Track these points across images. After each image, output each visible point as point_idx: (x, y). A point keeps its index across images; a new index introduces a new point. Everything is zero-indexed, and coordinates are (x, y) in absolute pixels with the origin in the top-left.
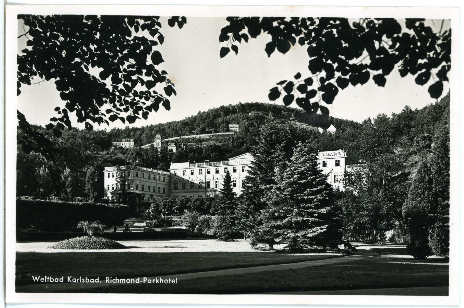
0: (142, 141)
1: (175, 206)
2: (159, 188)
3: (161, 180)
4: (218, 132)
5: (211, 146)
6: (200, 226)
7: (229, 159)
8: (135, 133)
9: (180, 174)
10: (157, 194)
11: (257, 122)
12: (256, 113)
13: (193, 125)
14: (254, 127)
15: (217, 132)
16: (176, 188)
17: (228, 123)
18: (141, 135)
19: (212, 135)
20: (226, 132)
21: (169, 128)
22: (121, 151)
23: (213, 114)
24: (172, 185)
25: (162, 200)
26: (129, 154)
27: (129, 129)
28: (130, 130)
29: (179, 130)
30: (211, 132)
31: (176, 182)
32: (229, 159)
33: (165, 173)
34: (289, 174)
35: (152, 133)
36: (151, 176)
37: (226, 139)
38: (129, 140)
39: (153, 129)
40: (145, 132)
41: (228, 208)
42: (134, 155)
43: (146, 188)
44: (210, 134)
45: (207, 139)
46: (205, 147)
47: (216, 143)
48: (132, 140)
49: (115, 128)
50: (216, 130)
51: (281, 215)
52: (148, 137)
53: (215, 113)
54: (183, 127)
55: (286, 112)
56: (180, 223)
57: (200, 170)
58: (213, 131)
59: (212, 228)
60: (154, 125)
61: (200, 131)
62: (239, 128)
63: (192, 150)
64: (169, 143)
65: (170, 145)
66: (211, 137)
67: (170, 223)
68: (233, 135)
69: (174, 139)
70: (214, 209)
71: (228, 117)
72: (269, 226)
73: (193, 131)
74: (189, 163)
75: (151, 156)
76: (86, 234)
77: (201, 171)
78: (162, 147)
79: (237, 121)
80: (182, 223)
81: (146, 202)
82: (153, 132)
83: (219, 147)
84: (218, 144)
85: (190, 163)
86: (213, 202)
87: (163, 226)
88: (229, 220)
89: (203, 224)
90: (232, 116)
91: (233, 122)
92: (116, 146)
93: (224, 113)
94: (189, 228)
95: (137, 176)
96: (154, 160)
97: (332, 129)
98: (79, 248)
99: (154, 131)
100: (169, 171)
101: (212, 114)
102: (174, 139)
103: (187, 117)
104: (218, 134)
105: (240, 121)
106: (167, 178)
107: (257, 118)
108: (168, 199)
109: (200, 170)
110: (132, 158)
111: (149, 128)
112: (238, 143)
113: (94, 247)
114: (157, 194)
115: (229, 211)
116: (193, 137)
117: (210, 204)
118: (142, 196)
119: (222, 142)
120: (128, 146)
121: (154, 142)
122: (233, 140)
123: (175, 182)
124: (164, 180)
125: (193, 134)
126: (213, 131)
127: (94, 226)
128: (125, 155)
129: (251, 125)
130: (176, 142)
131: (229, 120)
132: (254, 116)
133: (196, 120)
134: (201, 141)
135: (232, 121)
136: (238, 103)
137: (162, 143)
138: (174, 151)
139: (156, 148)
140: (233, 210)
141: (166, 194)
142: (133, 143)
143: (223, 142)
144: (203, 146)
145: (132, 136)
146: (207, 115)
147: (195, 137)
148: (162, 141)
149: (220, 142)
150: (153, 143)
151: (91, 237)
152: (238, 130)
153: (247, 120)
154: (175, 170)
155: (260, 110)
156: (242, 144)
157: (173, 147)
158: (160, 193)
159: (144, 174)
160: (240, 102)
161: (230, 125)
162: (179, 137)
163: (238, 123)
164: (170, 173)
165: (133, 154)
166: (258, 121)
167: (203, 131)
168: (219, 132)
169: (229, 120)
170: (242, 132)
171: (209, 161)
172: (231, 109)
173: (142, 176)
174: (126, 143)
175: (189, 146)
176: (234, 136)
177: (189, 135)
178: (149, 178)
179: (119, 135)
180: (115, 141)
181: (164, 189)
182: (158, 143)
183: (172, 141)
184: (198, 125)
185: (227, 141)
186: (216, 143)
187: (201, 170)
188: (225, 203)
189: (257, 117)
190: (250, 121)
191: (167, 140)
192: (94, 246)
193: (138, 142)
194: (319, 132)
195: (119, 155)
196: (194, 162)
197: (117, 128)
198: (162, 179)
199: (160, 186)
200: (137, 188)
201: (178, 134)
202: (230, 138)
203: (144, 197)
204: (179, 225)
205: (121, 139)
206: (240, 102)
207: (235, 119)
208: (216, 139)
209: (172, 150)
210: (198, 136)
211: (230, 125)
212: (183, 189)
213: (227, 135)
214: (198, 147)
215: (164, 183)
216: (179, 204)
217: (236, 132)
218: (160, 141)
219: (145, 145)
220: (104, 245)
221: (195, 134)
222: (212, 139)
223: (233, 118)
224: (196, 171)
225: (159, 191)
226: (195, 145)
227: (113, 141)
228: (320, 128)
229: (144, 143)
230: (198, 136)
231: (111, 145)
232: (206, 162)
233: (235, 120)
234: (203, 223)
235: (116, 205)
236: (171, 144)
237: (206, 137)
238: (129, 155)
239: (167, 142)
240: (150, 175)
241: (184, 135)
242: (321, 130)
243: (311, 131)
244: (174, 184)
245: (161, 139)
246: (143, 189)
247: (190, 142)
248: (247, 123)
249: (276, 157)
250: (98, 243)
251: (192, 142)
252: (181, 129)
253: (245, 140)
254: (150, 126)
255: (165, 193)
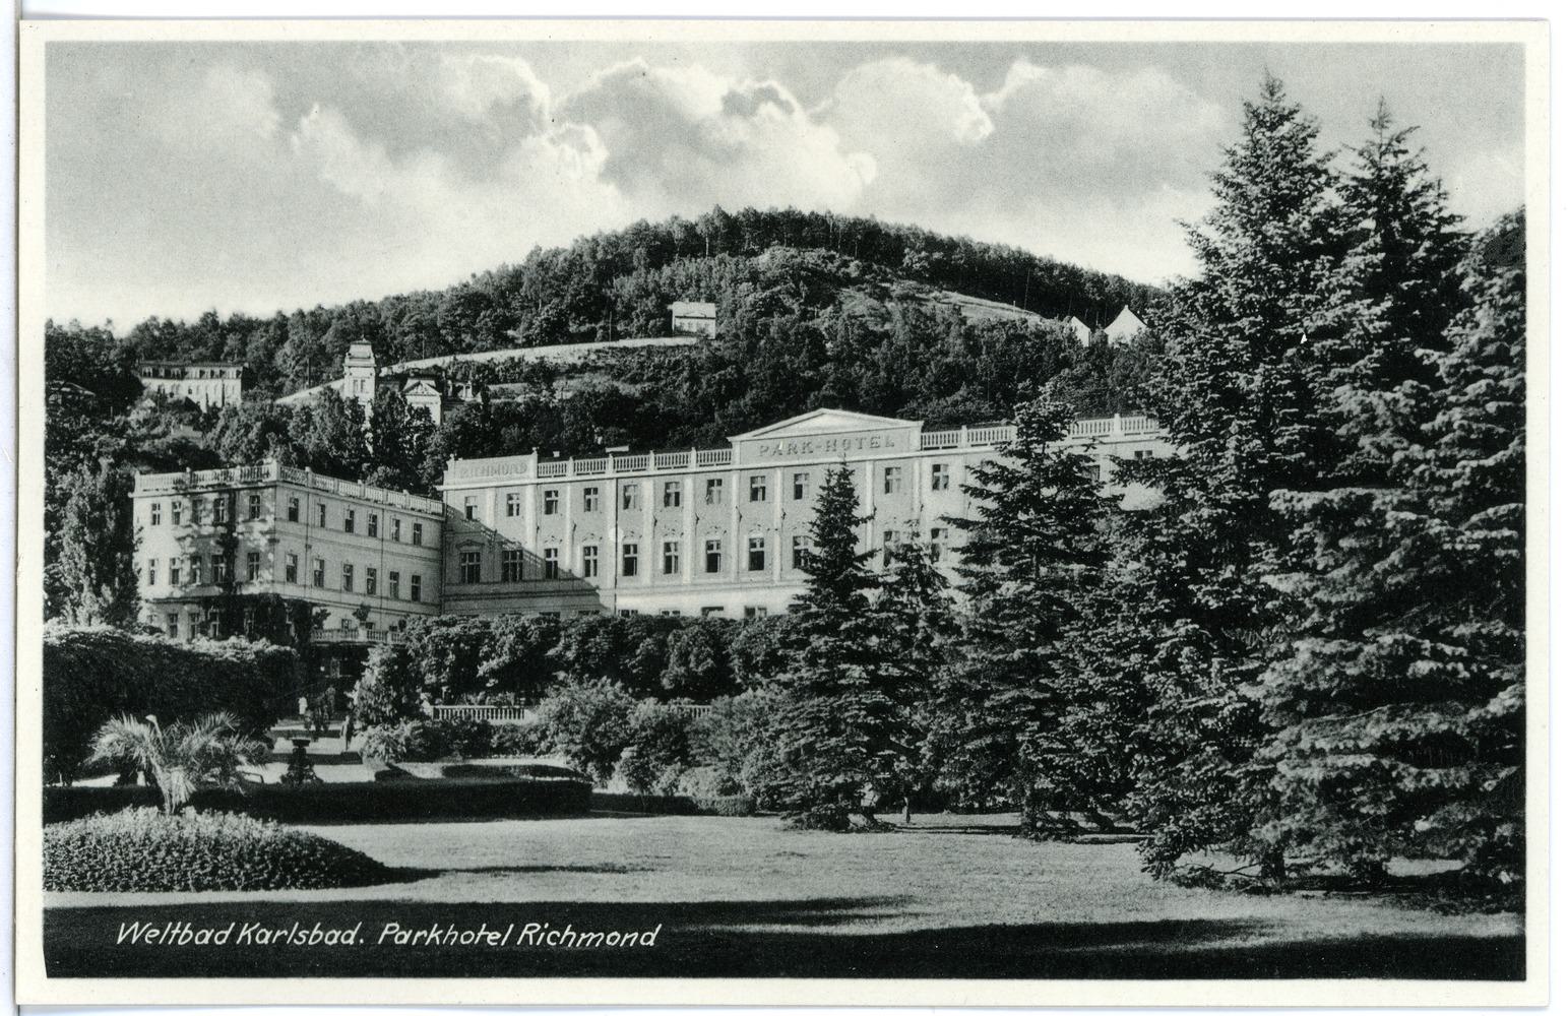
0: (278, 374)
1: (487, 657)
2: (394, 576)
3: (402, 539)
4: (623, 338)
5: (597, 395)
6: (640, 755)
7: (729, 439)
8: (244, 344)
9: (489, 515)
10: (385, 604)
11: (795, 294)
12: (793, 257)
13: (507, 306)
14: (783, 315)
15: (617, 336)
16: (473, 575)
17: (666, 299)
18: (271, 355)
19: (598, 351)
20: (657, 335)
21: (398, 319)
22: (188, 416)
23: (600, 256)
24: (454, 564)
25: (428, 631)
26: (226, 427)
27: (215, 324)
28: (223, 328)
29: (444, 326)
30: (589, 337)
31: (474, 548)
32: (729, 439)
33: (418, 502)
34: (1488, 418)
35: (323, 341)
36: (356, 515)
37: (660, 366)
38: (217, 370)
39: (328, 325)
40: (294, 337)
41: (853, 657)
42: (252, 435)
43: (334, 578)
44: (584, 347)
45: (574, 365)
46: (568, 401)
47: (616, 384)
48: (232, 371)
49: (154, 319)
50: (614, 329)
51: (1455, 672)
52: (306, 360)
53: (606, 252)
54: (463, 316)
55: (923, 254)
56: (533, 737)
57: (587, 491)
58: (600, 333)
59: (699, 764)
60: (326, 307)
61: (542, 330)
62: (718, 319)
63: (508, 415)
64: (410, 383)
65: (412, 388)
66: (593, 357)
67: (479, 739)
68: (690, 348)
69: (425, 364)
70: (682, 670)
71: (666, 270)
72: (1363, 745)
73: (510, 333)
74: (535, 455)
75: (334, 440)
76: (153, 796)
77: (592, 497)
78: (379, 396)
79: (708, 287)
80: (544, 737)
81: (337, 638)
82: (328, 337)
83: (629, 401)
84: (625, 388)
85: (539, 461)
86: (678, 638)
87: (449, 752)
88: (857, 716)
89: (649, 743)
90: (684, 268)
91: (692, 291)
92: (160, 398)
93: (649, 253)
94: (584, 764)
95: (293, 515)
96: (346, 454)
97: (1126, 327)
98: (154, 885)
99: (331, 331)
100: (438, 496)
101: (594, 257)
102: (425, 364)
103: (479, 275)
104: (622, 343)
105: (719, 287)
106: (430, 532)
107: (796, 278)
108: (453, 623)
109: (587, 491)
110: (243, 447)
111: (309, 319)
112: (719, 383)
113: (213, 873)
114: (385, 604)
115: (856, 672)
116: (512, 359)
117: (662, 644)
118: (316, 610)
119: (641, 381)
120: (215, 398)
121: (340, 375)
122: (692, 369)
123: (465, 549)
124: (417, 540)
125: (510, 342)
126: (600, 333)
127: (203, 748)
128: (210, 435)
129: (771, 306)
130: (437, 376)
131: (672, 284)
132: (783, 266)
133: (521, 285)
134: (545, 374)
135: (684, 288)
136: (710, 211)
137: (379, 380)
138: (436, 415)
139: (354, 401)
140: (878, 668)
141: (424, 604)
142: (238, 383)
143: (649, 380)
144: (558, 395)
145: (230, 354)
146: (572, 264)
147: (521, 359)
148: (378, 370)
149: (633, 381)
150: (335, 385)
151: (178, 810)
152: (712, 329)
153: (755, 284)
154: (467, 493)
155: (814, 244)
156: (737, 387)
157: (425, 397)
158: (396, 597)
159: (323, 507)
160: (718, 208)
161: (677, 308)
162: (448, 359)
163: (710, 299)
164: (446, 507)
165: (248, 428)
166: (804, 289)
167: (554, 333)
168: (628, 335)
169: (672, 284)
170: (736, 336)
171: (626, 449)
172: (678, 235)
173: (318, 521)
174: (202, 383)
175: (496, 396)
176: (694, 354)
177: (493, 349)
178: (349, 526)
179: (173, 349)
180: (156, 375)
181: (416, 579)
182: (358, 379)
183: (420, 375)
184: (531, 304)
185: (667, 375)
186: (616, 384)
187: (596, 490)
188: (830, 629)
189: (796, 273)
190: (764, 289)
191: (397, 369)
192: (216, 868)
193: (260, 377)
194: (1072, 339)
195: (182, 431)
196: (556, 454)
197: (161, 321)
198: (406, 532)
199: (393, 564)
200: (291, 574)
201: (445, 342)
202: (677, 363)
203: (324, 615)
204: (530, 749)
205: (183, 368)
206: (718, 208)
207: (698, 281)
208: (612, 367)
209: (425, 412)
210: (531, 355)
211: (677, 308)
212: (505, 579)
213: (666, 350)
214: (537, 402)
215: (417, 551)
216: (512, 651)
217: (702, 335)
218: (372, 371)
219: (293, 391)
220: (274, 860)
221: (516, 346)
222: (595, 369)
223: (689, 277)
224: (569, 497)
225: (395, 588)
226: (520, 394)
227: (146, 375)
228: (1076, 322)
229: (288, 384)
230: (531, 355)
231: (135, 391)
232: (615, 454)
233: (698, 286)
234: (654, 738)
235: (234, 647)
236: (418, 384)
237: (571, 360)
238: (228, 433)
239: (402, 378)
240: (352, 513)
241: (469, 349)
242: (1083, 334)
243: (1040, 335)
244: (464, 557)
245: (372, 361)
246: (319, 579)
247: (496, 380)
248: (750, 296)
249: (1322, 333)
250: (234, 853)
251: (506, 381)
252: (453, 324)
253: (747, 371)
254: (312, 314)
255: (423, 596)
